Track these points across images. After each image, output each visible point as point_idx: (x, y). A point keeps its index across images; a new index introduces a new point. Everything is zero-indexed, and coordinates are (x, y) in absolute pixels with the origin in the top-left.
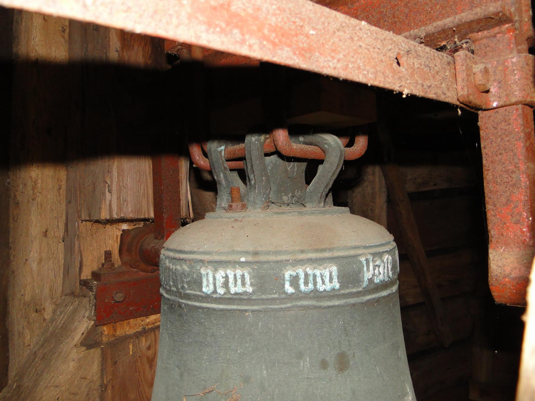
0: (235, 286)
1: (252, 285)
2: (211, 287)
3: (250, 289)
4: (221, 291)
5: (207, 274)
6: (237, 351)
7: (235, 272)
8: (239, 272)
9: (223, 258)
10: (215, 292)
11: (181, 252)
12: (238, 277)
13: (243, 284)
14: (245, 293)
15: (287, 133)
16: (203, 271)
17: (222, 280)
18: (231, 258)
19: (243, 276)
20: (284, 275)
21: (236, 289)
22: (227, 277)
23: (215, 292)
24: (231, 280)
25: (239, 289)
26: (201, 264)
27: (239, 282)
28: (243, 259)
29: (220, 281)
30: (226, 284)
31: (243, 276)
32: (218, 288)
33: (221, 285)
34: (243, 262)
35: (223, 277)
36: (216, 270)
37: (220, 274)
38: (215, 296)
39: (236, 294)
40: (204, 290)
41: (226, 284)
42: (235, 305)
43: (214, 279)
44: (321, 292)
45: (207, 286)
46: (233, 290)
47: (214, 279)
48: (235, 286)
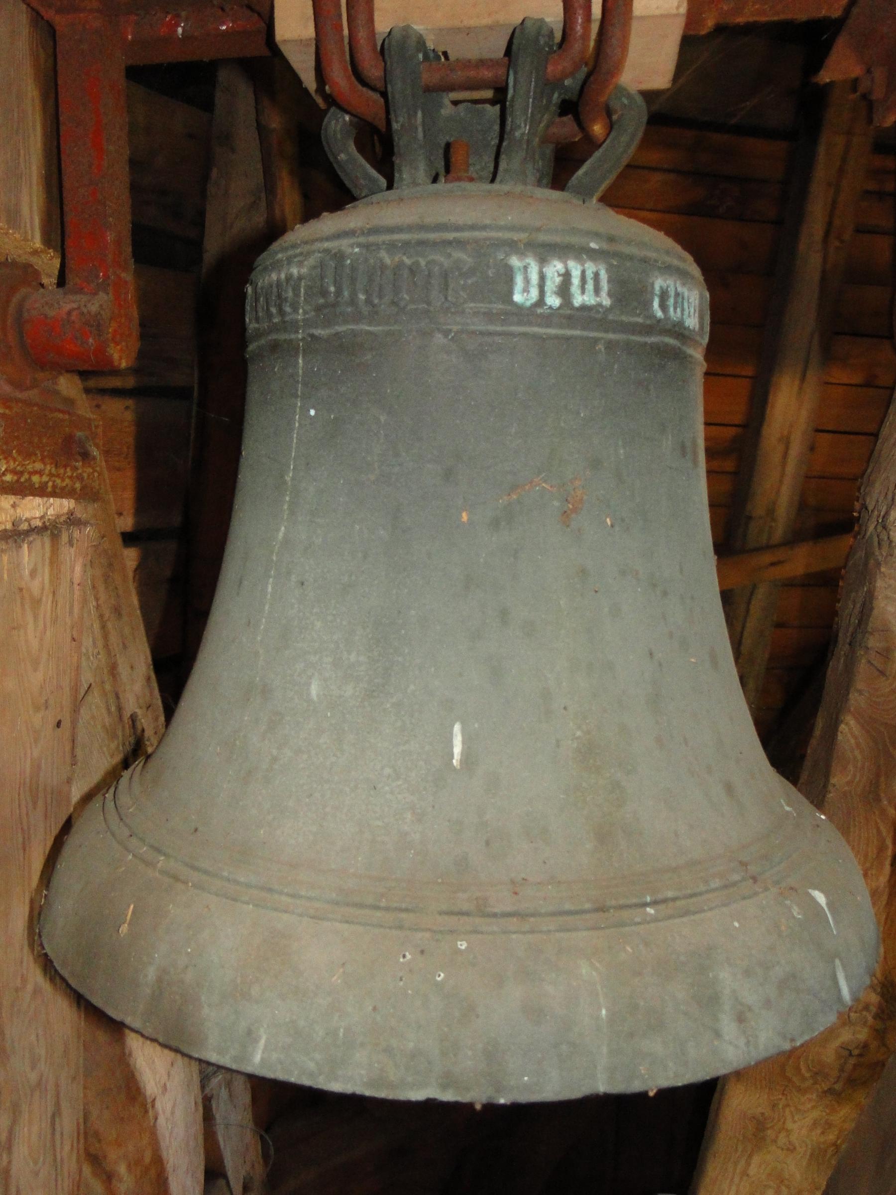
0: (583, 291)
1: (610, 294)
2: (534, 293)
3: (606, 302)
4: (553, 301)
5: (526, 268)
6: (578, 413)
7: (583, 265)
8: (591, 268)
9: (557, 239)
10: (541, 302)
11: (458, 228)
12: (589, 274)
13: (597, 290)
14: (600, 305)
15: (254, 273)
16: (515, 262)
17: (558, 280)
18: (575, 240)
19: (596, 275)
20: (653, 284)
21: (586, 298)
22: (567, 276)
23: (541, 302)
24: (576, 281)
25: (589, 299)
26: (507, 249)
27: (590, 286)
28: (593, 245)
29: (554, 282)
30: (564, 290)
31: (596, 275)
32: (548, 294)
33: (555, 289)
34: (593, 250)
35: (559, 275)
36: (543, 261)
37: (554, 269)
38: (539, 311)
39: (584, 308)
40: (518, 298)
41: (564, 290)
42: (577, 329)
43: (542, 278)
44: (685, 328)
45: (526, 290)
46: (578, 300)
47: (542, 278)
48: (583, 291)
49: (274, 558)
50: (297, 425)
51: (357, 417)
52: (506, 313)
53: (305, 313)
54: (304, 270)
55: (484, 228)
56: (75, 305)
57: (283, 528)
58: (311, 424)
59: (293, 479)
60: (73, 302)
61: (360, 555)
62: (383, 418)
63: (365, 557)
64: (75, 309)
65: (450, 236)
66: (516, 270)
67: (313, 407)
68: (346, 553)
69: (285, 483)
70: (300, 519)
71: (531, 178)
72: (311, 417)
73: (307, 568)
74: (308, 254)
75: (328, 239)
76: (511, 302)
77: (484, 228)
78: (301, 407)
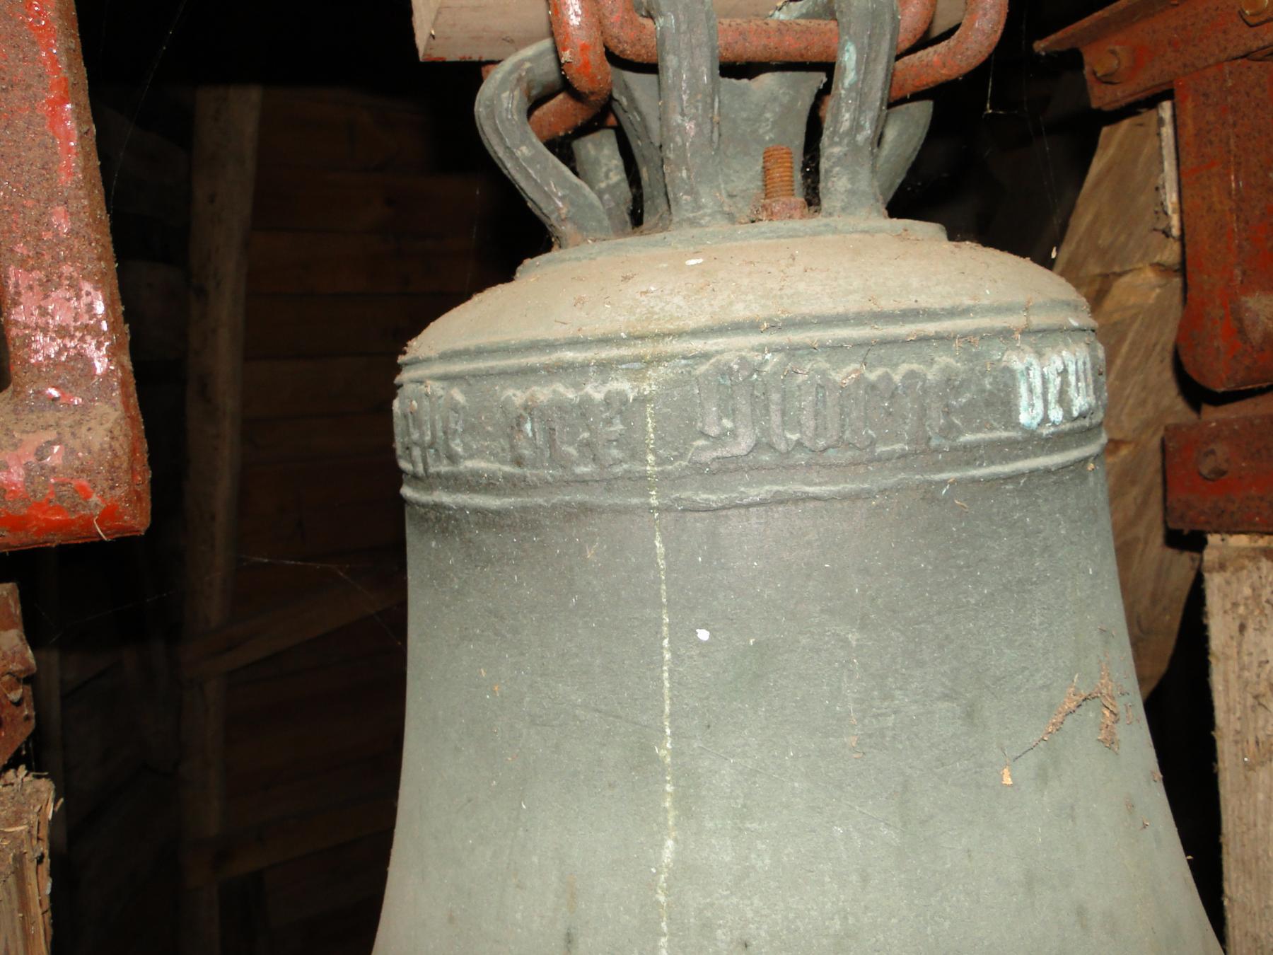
10: (1045, 419)
40: (1024, 418)
49: (662, 899)
50: (667, 656)
51: (804, 640)
52: (1011, 443)
53: (661, 461)
54: (647, 388)
55: (965, 312)
56: (51, 435)
57: (670, 843)
58: (702, 655)
59: (676, 753)
60: (46, 428)
61: (854, 878)
62: (853, 638)
63: (865, 879)
64: (51, 444)
65: (931, 328)
66: (1019, 376)
67: (705, 626)
68: (827, 879)
69: (656, 759)
70: (709, 825)
71: (797, 213)
72: (700, 643)
73: (750, 915)
74: (658, 360)
75: (696, 333)
76: (1017, 425)
77: (965, 312)
78: (669, 625)
